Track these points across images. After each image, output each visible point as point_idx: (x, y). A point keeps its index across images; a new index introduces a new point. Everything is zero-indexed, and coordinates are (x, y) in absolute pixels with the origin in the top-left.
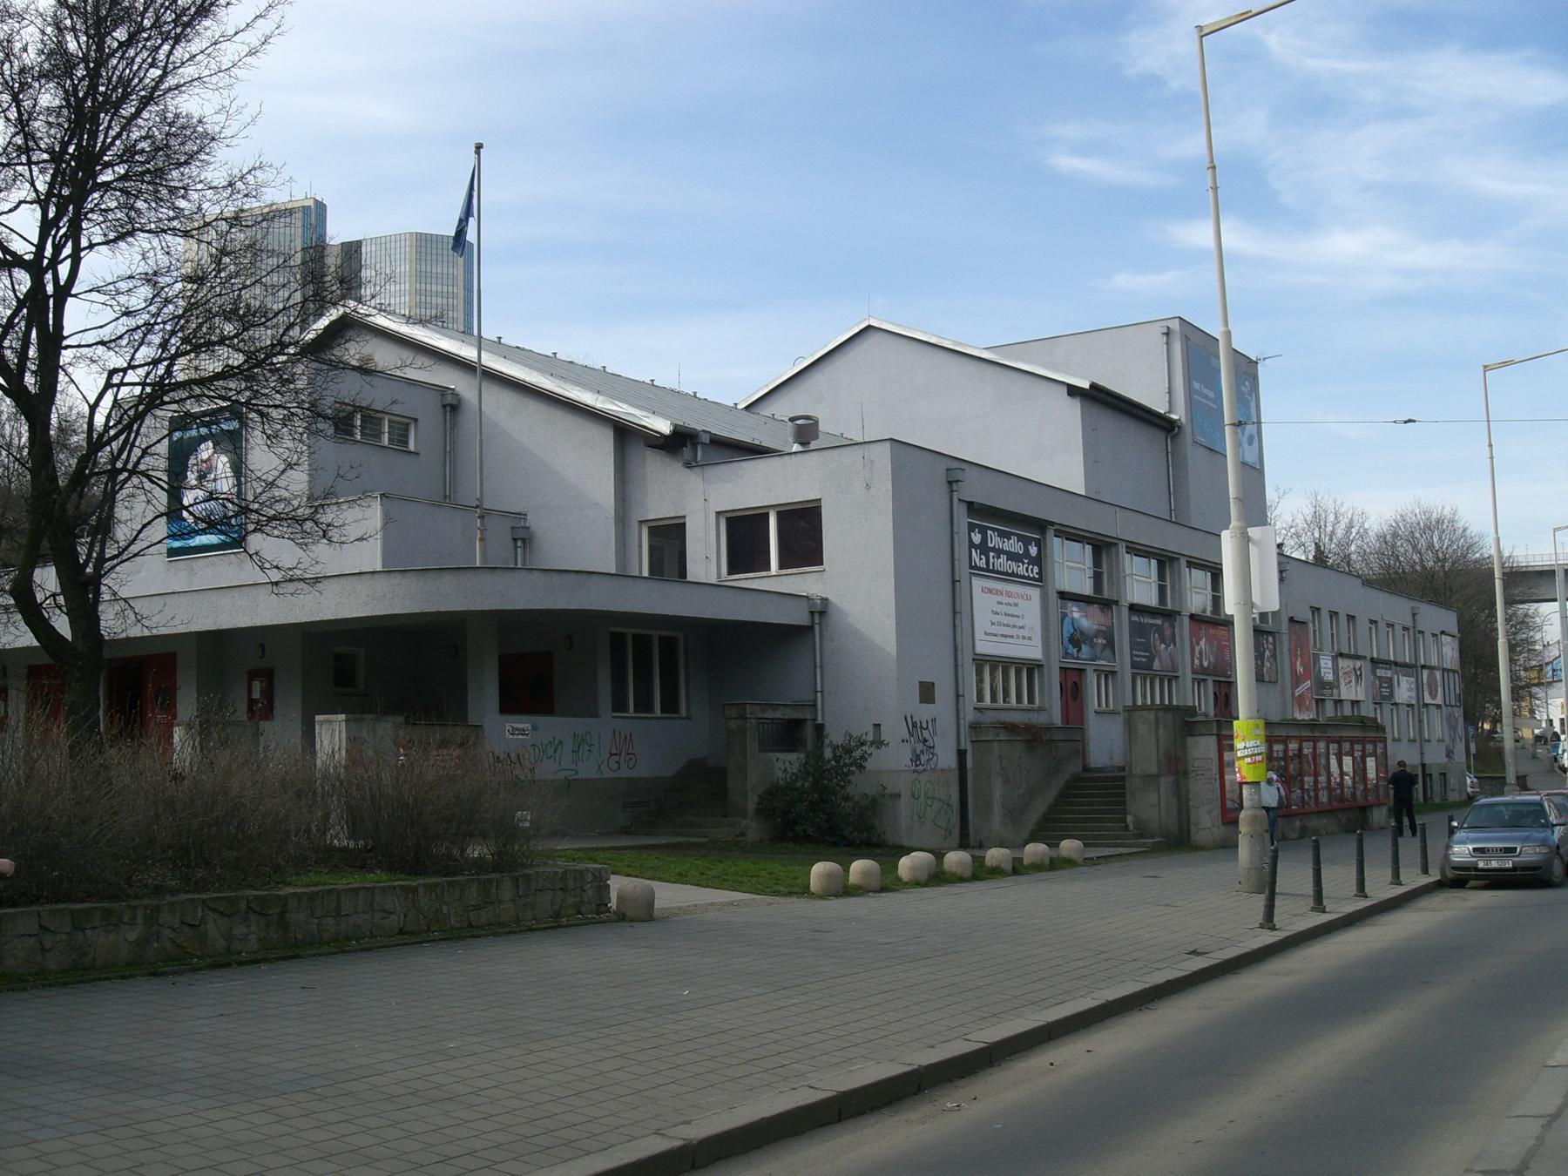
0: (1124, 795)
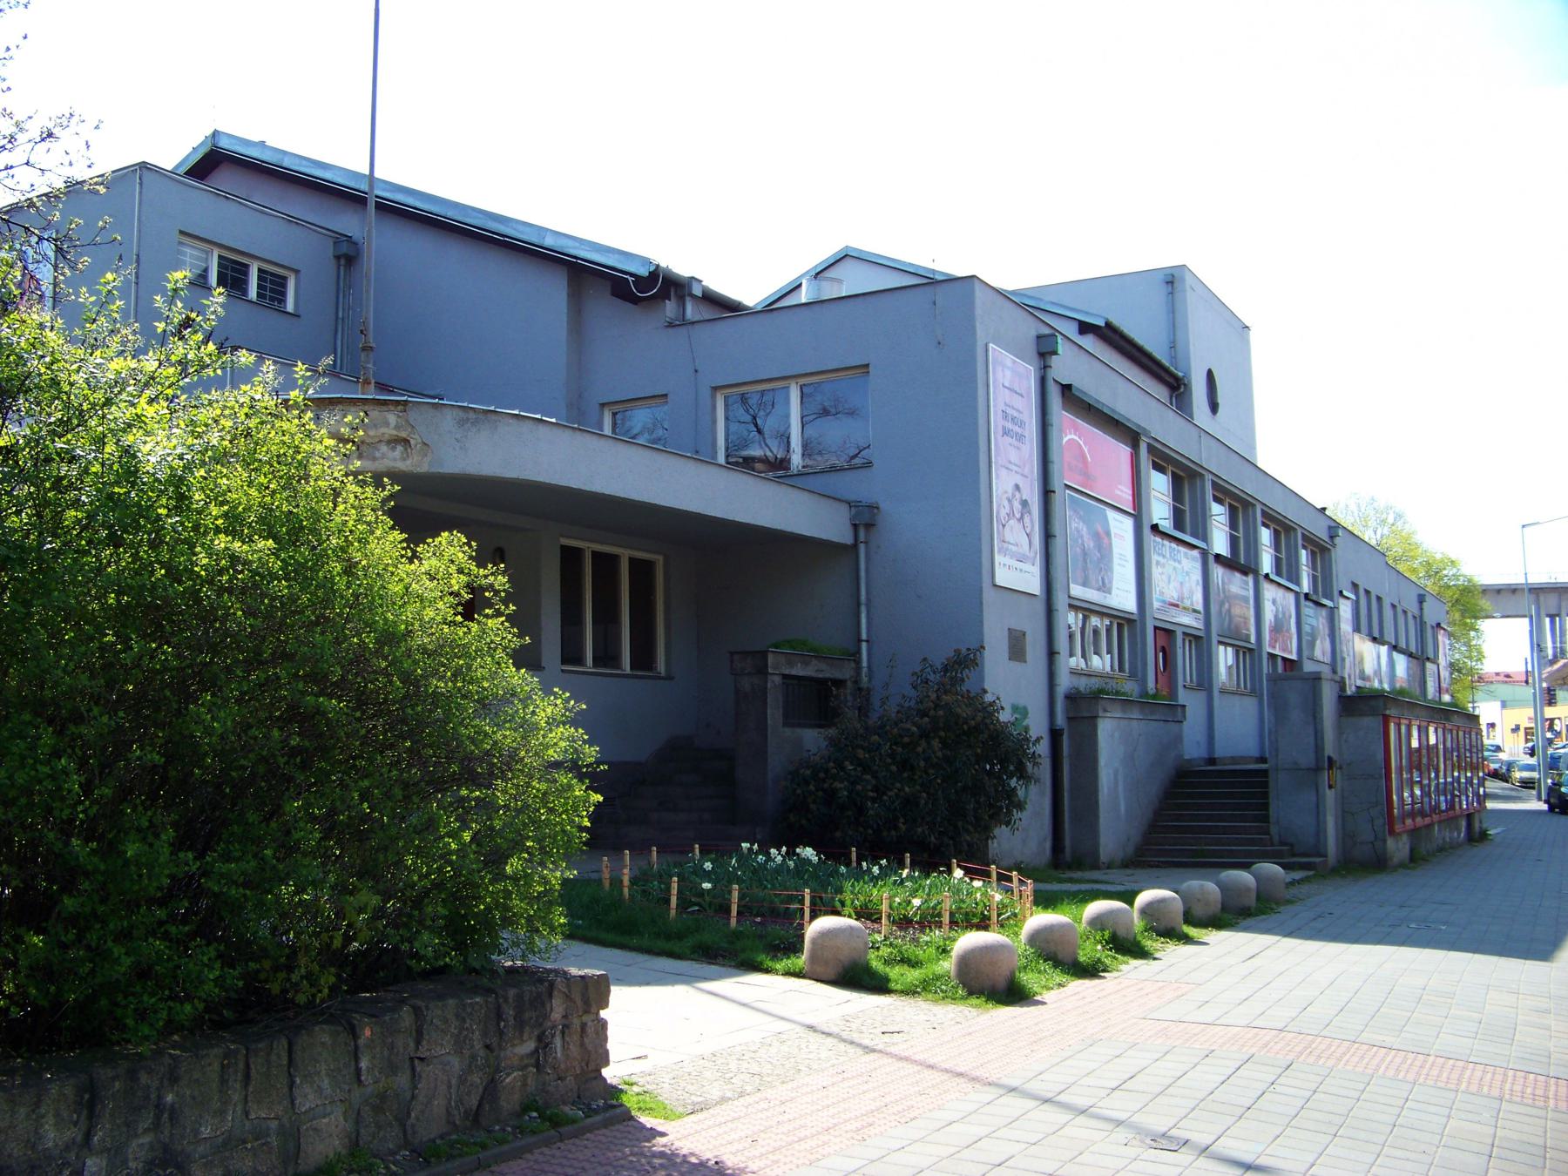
0: (1265, 795)
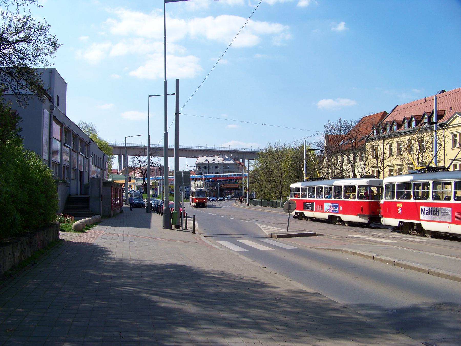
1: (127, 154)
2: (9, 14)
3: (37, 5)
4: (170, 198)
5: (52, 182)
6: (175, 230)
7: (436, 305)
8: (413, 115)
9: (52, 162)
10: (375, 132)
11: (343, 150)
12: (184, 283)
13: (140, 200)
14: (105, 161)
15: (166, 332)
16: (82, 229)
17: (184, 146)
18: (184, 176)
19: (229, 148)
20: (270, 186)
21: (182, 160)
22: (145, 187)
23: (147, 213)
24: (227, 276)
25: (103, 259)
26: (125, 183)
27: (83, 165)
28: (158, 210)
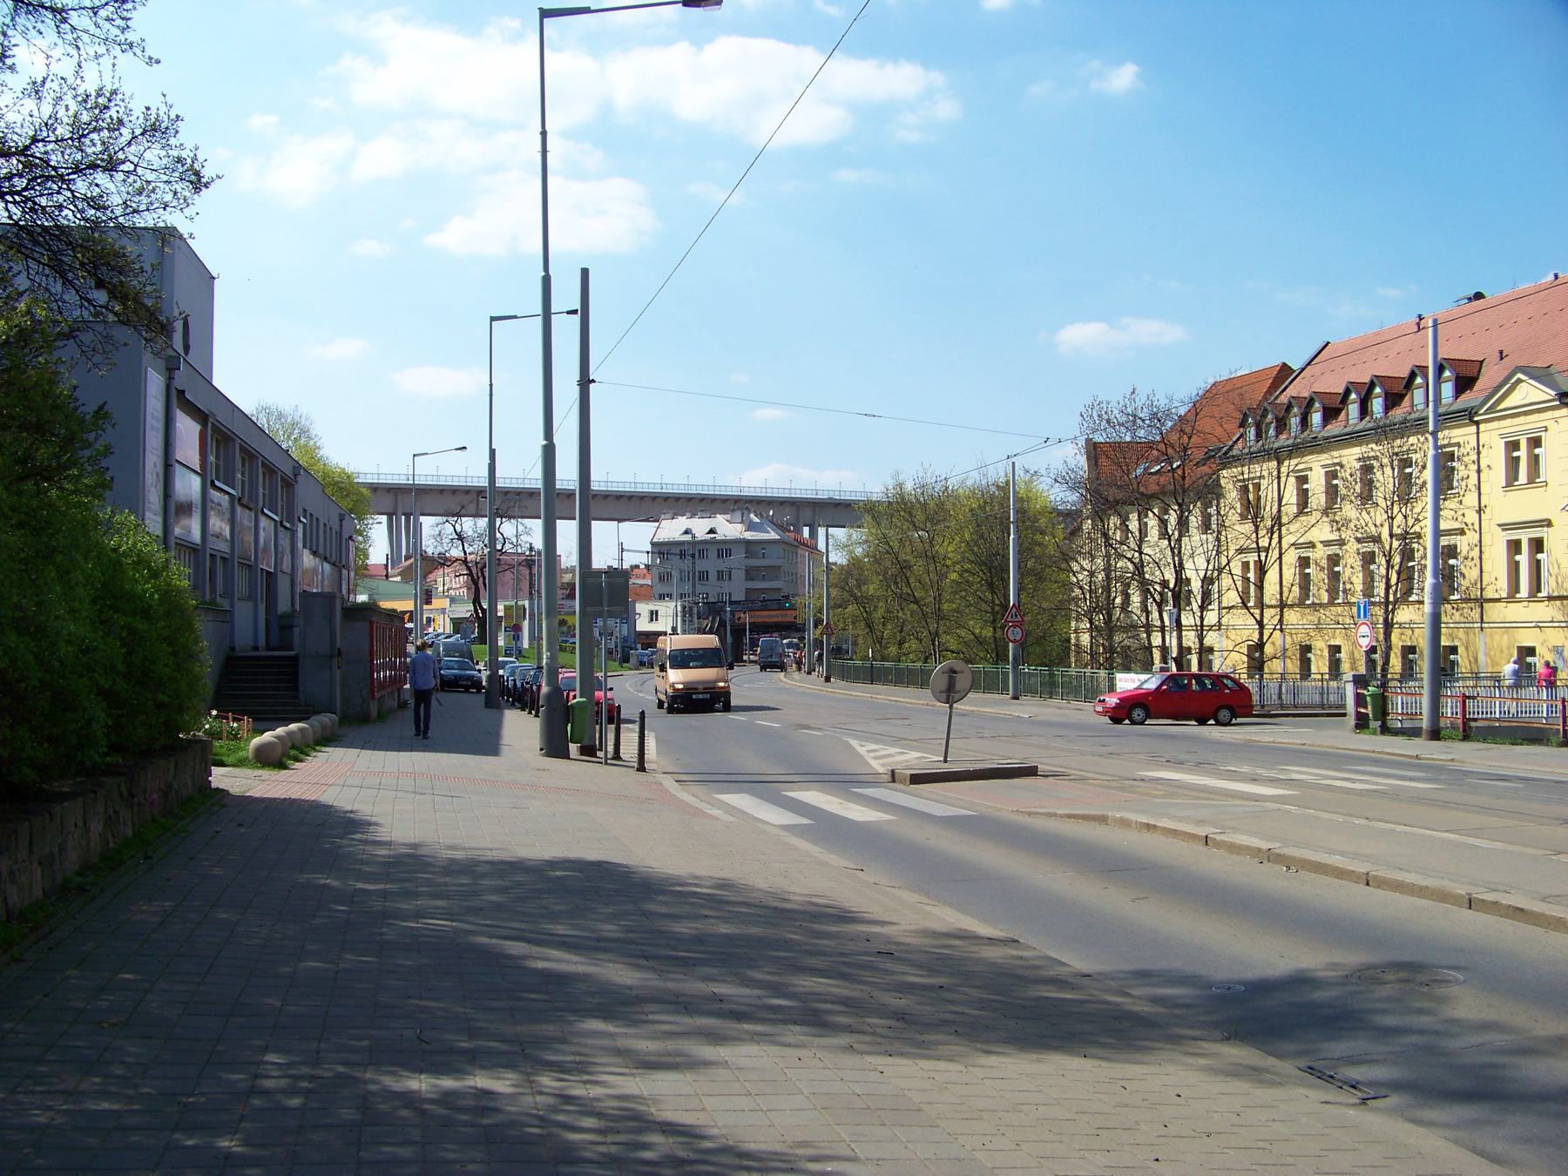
0: (296, 673)
1: (418, 513)
2: (52, 81)
3: (143, 56)
4: (563, 658)
5: (188, 609)
6: (579, 760)
7: (1368, 969)
8: (1376, 376)
9: (176, 543)
10: (1252, 433)
11: (1142, 494)
12: (606, 911)
13: (463, 666)
14: (345, 536)
15: (550, 1029)
16: (281, 759)
17: (610, 484)
18: (607, 583)
19: (764, 490)
20: (899, 615)
21: (601, 531)
22: (482, 623)
23: (489, 707)
24: (736, 892)
25: (355, 845)
26: (412, 609)
27: (273, 549)
28: (523, 698)
